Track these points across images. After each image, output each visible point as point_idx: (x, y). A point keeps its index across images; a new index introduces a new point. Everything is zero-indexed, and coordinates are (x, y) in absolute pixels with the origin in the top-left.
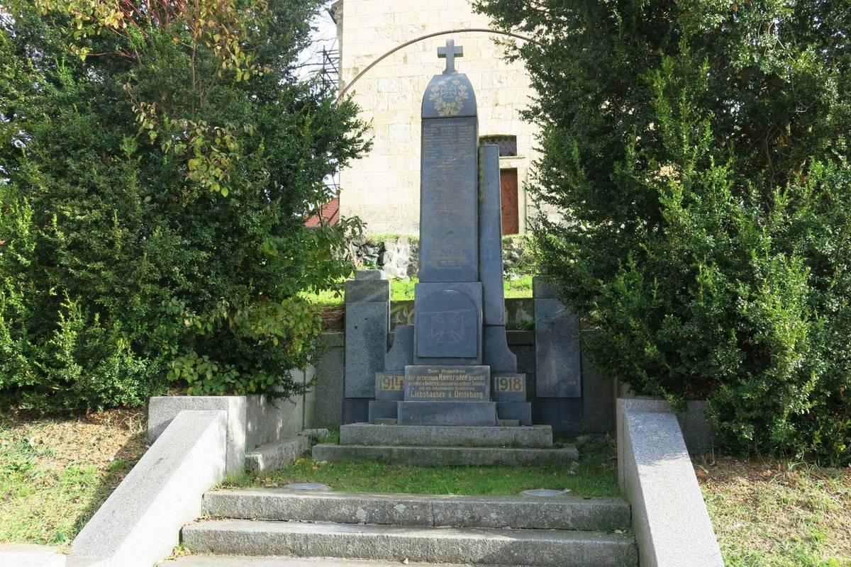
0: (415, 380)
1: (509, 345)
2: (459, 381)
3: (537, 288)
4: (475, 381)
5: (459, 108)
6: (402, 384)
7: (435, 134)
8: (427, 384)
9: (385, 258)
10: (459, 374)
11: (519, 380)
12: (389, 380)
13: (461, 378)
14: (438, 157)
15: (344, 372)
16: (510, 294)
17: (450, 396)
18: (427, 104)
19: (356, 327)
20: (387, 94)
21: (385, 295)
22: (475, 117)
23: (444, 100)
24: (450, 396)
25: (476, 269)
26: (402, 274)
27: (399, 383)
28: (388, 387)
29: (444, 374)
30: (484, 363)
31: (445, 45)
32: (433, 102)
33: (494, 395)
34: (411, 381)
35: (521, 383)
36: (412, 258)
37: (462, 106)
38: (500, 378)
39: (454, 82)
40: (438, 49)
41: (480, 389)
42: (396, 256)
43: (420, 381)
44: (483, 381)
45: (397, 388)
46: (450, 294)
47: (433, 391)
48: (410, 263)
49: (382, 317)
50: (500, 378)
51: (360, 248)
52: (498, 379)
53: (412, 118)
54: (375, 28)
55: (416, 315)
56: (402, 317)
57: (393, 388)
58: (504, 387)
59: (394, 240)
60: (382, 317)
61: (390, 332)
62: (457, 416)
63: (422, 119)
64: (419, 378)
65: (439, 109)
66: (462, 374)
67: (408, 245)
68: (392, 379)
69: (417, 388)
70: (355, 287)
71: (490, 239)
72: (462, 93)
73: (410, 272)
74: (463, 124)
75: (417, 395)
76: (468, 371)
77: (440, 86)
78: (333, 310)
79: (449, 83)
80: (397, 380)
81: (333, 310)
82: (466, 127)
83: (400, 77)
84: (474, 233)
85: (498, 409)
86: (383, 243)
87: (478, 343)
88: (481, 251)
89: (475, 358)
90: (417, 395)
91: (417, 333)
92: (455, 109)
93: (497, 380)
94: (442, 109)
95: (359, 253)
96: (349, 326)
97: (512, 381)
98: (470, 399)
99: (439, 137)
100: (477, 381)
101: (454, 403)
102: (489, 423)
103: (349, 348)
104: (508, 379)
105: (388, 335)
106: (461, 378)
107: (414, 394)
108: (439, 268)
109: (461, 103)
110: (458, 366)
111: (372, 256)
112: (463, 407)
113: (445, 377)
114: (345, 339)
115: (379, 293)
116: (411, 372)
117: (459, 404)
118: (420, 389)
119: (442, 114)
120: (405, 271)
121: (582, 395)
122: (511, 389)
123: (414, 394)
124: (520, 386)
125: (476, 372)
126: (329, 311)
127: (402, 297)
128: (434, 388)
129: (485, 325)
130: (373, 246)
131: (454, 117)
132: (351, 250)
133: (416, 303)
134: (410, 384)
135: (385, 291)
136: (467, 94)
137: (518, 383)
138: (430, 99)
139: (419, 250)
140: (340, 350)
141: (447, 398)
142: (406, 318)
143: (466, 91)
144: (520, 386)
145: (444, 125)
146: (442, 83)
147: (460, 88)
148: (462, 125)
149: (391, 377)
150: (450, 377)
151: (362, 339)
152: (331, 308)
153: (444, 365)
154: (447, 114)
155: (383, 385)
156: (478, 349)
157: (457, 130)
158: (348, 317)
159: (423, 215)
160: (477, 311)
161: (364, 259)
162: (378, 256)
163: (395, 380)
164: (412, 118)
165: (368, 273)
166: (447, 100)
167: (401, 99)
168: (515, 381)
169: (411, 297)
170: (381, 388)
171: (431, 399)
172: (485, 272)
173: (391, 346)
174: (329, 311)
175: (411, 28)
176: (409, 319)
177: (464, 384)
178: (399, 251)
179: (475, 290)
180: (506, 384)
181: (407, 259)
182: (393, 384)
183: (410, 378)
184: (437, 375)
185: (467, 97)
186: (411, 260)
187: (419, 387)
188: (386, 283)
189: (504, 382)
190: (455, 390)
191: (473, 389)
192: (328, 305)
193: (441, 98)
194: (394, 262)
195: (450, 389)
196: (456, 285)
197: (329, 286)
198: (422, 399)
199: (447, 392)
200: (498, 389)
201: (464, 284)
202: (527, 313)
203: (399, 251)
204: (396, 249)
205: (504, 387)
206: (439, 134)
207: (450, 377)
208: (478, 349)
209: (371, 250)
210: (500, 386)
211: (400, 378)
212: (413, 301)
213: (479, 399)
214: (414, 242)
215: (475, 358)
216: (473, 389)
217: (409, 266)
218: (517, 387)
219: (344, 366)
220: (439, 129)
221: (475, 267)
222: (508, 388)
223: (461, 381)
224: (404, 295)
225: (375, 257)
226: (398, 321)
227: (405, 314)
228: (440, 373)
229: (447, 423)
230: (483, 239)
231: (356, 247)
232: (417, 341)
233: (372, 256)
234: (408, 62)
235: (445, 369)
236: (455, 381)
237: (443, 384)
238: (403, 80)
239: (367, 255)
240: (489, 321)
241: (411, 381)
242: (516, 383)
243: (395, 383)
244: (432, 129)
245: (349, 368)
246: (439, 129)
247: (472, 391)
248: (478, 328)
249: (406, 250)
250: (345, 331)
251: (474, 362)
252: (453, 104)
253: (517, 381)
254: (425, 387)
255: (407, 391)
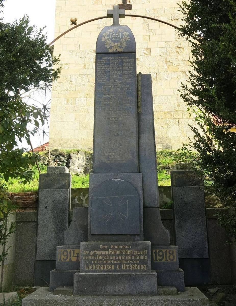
0: (89, 255)
1: (162, 220)
2: (126, 255)
3: (174, 178)
4: (139, 255)
5: (124, 47)
6: (78, 257)
7: (105, 64)
8: (99, 258)
9: (71, 163)
10: (125, 249)
11: (173, 253)
12: (67, 253)
13: (127, 252)
14: (107, 80)
15: (36, 240)
16: (161, 184)
17: (118, 268)
18: (100, 43)
19: (46, 207)
20: (75, 83)
21: (67, 184)
22: (134, 53)
23: (112, 41)
24: (118, 268)
25: (138, 162)
26: (81, 172)
27: (75, 255)
28: (66, 259)
29: (114, 249)
30: (146, 239)
31: (112, 9)
32: (105, 42)
33: (154, 267)
34: (86, 256)
35: (175, 254)
36: (87, 163)
37: (126, 46)
38: (158, 251)
39: (119, 30)
40: (108, 11)
41: (143, 262)
42: (77, 162)
43: (93, 255)
44: (145, 255)
45: (74, 259)
46: (117, 182)
47: (104, 264)
48: (86, 166)
49: (65, 199)
50: (158, 251)
51: (56, 157)
52: (156, 251)
53: (87, 95)
54: (70, 51)
55: (90, 199)
56: (79, 199)
57: (70, 259)
58: (161, 258)
59: (76, 152)
60: (65, 199)
61: (70, 211)
62: (125, 287)
63: (96, 53)
64: (92, 253)
65: (109, 47)
66: (129, 249)
67: (85, 156)
68: (70, 253)
69: (90, 262)
70: (46, 178)
71: (147, 141)
72: (126, 37)
73: (86, 171)
74: (126, 58)
75: (90, 268)
76: (132, 246)
77: (110, 32)
78: (30, 195)
79: (116, 31)
80: (74, 253)
81: (30, 195)
82: (128, 60)
83: (82, 75)
84: (135, 135)
85: (159, 277)
86: (70, 154)
87: (140, 222)
88: (140, 150)
89: (138, 235)
90: (90, 268)
91: (91, 214)
92: (121, 47)
93: (155, 253)
94: (111, 47)
95: (55, 160)
96: (41, 207)
97: (168, 253)
98: (136, 271)
99: (108, 66)
100: (141, 255)
101: (122, 275)
102: (153, 294)
103: (40, 222)
104: (164, 251)
105: (69, 212)
106: (127, 252)
107: (88, 267)
108: (109, 162)
109: (125, 43)
110: (124, 242)
111: (63, 162)
112: (132, 279)
113: (114, 252)
114: (38, 216)
115: (64, 183)
116: (86, 248)
117: (126, 276)
118: (93, 262)
119: (110, 51)
120: (83, 171)
121: (209, 256)
122: (166, 260)
123: (88, 267)
124: (174, 257)
125: (140, 247)
126: (28, 195)
127: (79, 186)
128: (104, 262)
129: (145, 207)
130: (64, 156)
131: (119, 53)
132: (50, 157)
133: (90, 190)
134: (84, 258)
135: (67, 181)
136: (129, 37)
137: (172, 254)
138: (102, 40)
139: (91, 158)
140: (34, 223)
141: (115, 270)
142: (83, 200)
143: (129, 36)
144: (174, 257)
145: (113, 58)
146: (111, 30)
147: (123, 33)
148: (125, 58)
149: (69, 251)
150: (119, 252)
151: (50, 216)
152: (30, 193)
153: (113, 241)
154: (115, 51)
155: (63, 257)
156: (140, 227)
157: (122, 62)
158: (40, 200)
159: (96, 122)
160: (139, 196)
161: (58, 163)
162: (66, 161)
163: (72, 252)
164: (87, 95)
165: (56, 168)
166: (115, 41)
167: (82, 85)
168: (169, 252)
169: (87, 185)
170: (60, 260)
171: (101, 271)
172: (143, 166)
173: (71, 221)
174: (28, 195)
175: (88, 51)
176: (84, 201)
177: (130, 258)
178: (79, 159)
179: (137, 179)
180: (163, 255)
181: (83, 163)
182: (70, 256)
183: (85, 253)
184: (107, 250)
185: (129, 40)
186: (86, 164)
187: (92, 260)
188: (69, 175)
189: (161, 253)
190: (122, 263)
191: (138, 262)
192: (28, 191)
193: (110, 40)
194: (76, 165)
195: (118, 262)
196: (122, 175)
197: (18, 174)
198: (95, 271)
199: (115, 265)
200: (156, 260)
201: (129, 174)
202: (167, 197)
203: (79, 159)
204: (77, 158)
205: (161, 258)
206: (108, 64)
207: (119, 252)
208: (140, 227)
209: (62, 158)
210: (158, 257)
211: (76, 251)
212: (88, 188)
213: (143, 271)
214: (88, 154)
215: (138, 235)
216: (138, 262)
217: (85, 168)
218: (172, 257)
219: (37, 236)
220: (108, 60)
221: (136, 161)
222: (165, 258)
223: (128, 255)
224: (81, 184)
225: (64, 162)
226: (77, 202)
227: (81, 198)
228: (110, 248)
229: (116, 293)
230: (142, 141)
231: (53, 156)
232: (91, 220)
233: (63, 162)
234: (86, 68)
235: (114, 245)
236: (122, 255)
237: (112, 258)
238: (84, 76)
239: (60, 161)
240: (147, 205)
241: (86, 256)
242: (170, 254)
243: (72, 256)
244: (103, 61)
245: (40, 238)
246: (108, 60)
247: (137, 264)
248: (140, 209)
249: (83, 158)
250: (38, 210)
251: (138, 238)
252: (119, 44)
253: (171, 252)
254: (98, 260)
255: (82, 264)
